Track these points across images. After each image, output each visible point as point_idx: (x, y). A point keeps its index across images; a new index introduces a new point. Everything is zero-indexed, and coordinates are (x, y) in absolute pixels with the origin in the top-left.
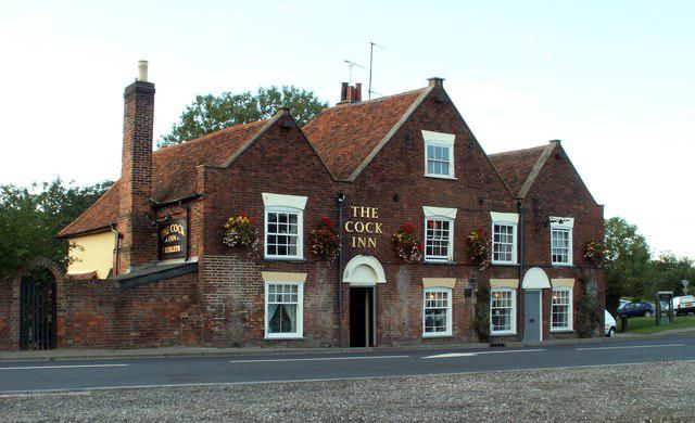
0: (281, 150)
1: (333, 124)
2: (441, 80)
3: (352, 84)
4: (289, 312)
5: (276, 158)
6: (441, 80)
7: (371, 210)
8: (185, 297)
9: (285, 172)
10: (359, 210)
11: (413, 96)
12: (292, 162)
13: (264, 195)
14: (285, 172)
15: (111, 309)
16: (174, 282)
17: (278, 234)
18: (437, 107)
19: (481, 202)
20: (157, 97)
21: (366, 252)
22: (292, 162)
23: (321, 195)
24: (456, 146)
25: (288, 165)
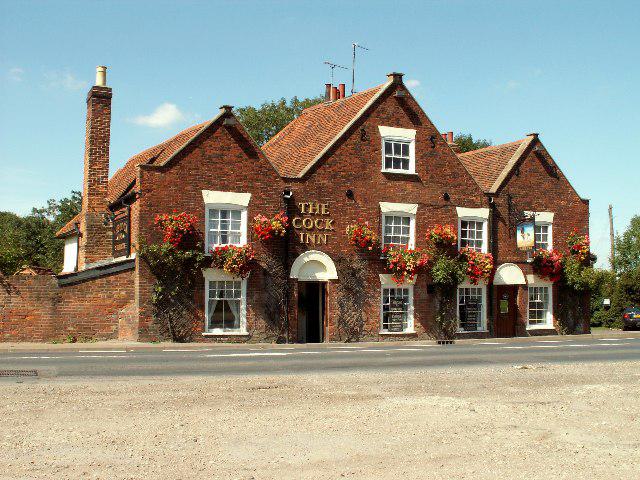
0: (222, 149)
1: (307, 123)
2: (537, 135)
3: (336, 85)
4: (233, 307)
5: (218, 157)
6: (537, 135)
7: (320, 206)
8: (123, 293)
9: (227, 169)
10: (307, 207)
11: (515, 147)
12: (234, 159)
13: (205, 192)
14: (227, 169)
15: (49, 305)
16: (112, 278)
17: (401, 235)
18: (397, 103)
19: (446, 198)
20: (113, 100)
21: (320, 247)
22: (234, 159)
23: (265, 192)
24: (417, 141)
25: (230, 163)
